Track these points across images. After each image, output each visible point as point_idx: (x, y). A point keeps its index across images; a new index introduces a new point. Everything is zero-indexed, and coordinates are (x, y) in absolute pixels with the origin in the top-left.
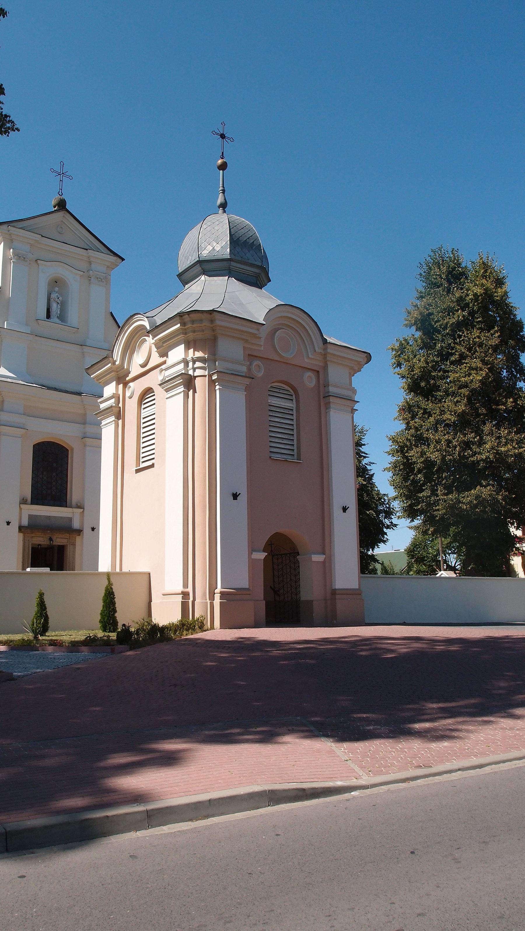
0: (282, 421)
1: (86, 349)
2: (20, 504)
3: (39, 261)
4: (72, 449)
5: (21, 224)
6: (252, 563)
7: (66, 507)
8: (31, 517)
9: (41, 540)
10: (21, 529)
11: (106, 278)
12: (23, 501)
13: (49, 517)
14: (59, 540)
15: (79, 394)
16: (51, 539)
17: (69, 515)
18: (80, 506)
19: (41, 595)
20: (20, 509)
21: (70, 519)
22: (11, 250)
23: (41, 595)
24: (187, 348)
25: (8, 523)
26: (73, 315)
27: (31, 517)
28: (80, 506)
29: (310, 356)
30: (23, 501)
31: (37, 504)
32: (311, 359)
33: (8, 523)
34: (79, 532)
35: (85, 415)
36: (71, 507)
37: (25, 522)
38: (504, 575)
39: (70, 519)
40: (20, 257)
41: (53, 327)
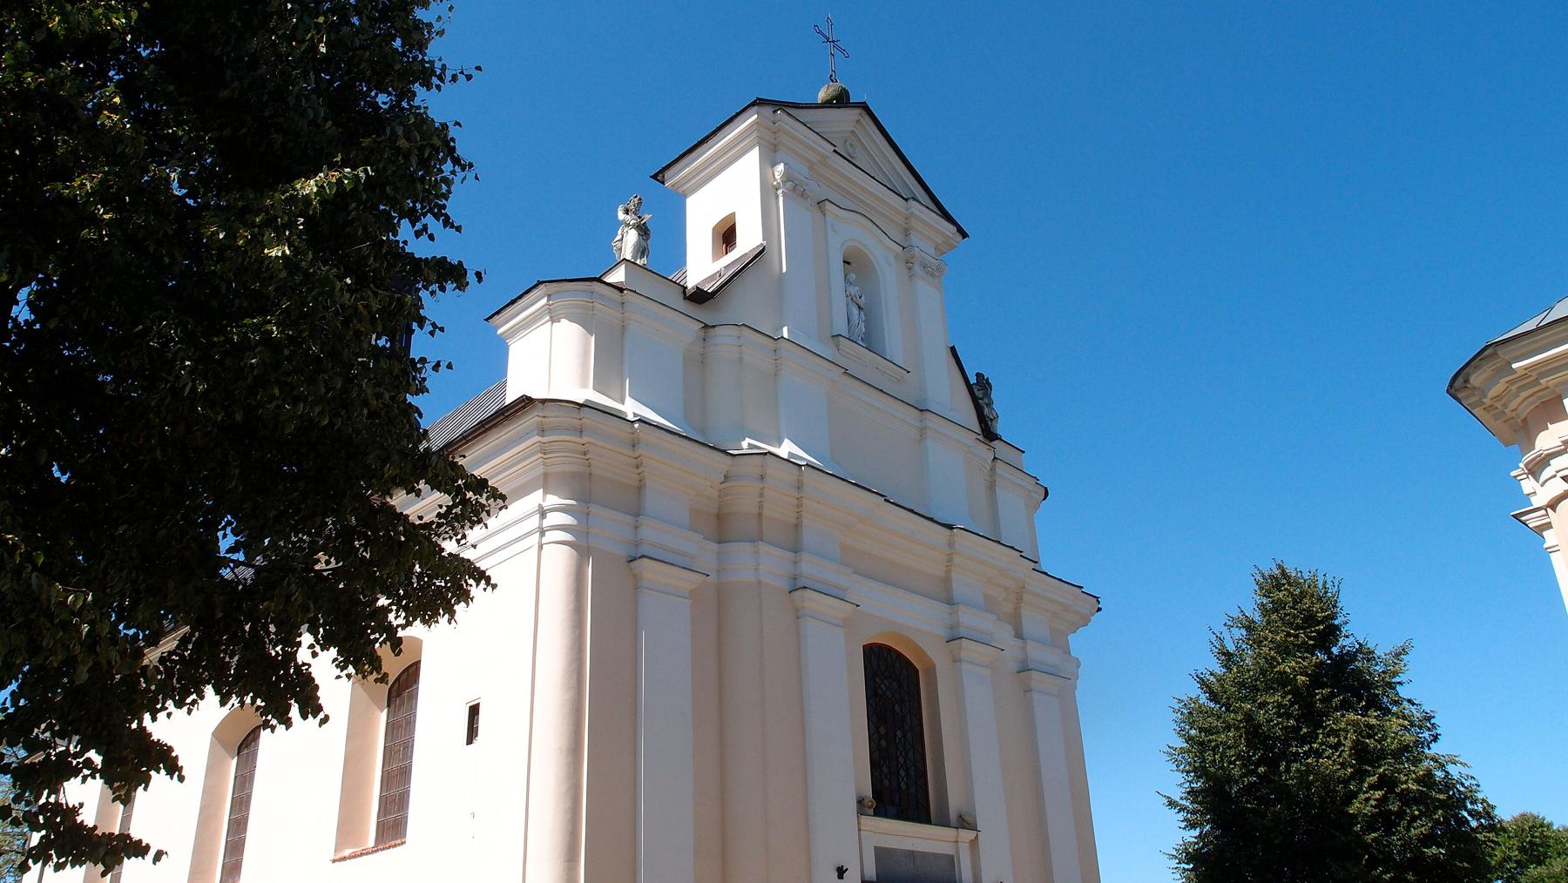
1: (932, 422)
3: (828, 206)
4: (931, 669)
5: (791, 111)
7: (928, 821)
8: (881, 853)
11: (939, 269)
13: (912, 854)
15: (950, 527)
17: (944, 848)
18: (965, 822)
21: (951, 860)
22: (781, 167)
24: (545, 493)
27: (881, 853)
28: (965, 822)
31: (886, 815)
36: (944, 822)
38: (920, 821)
40: (796, 188)
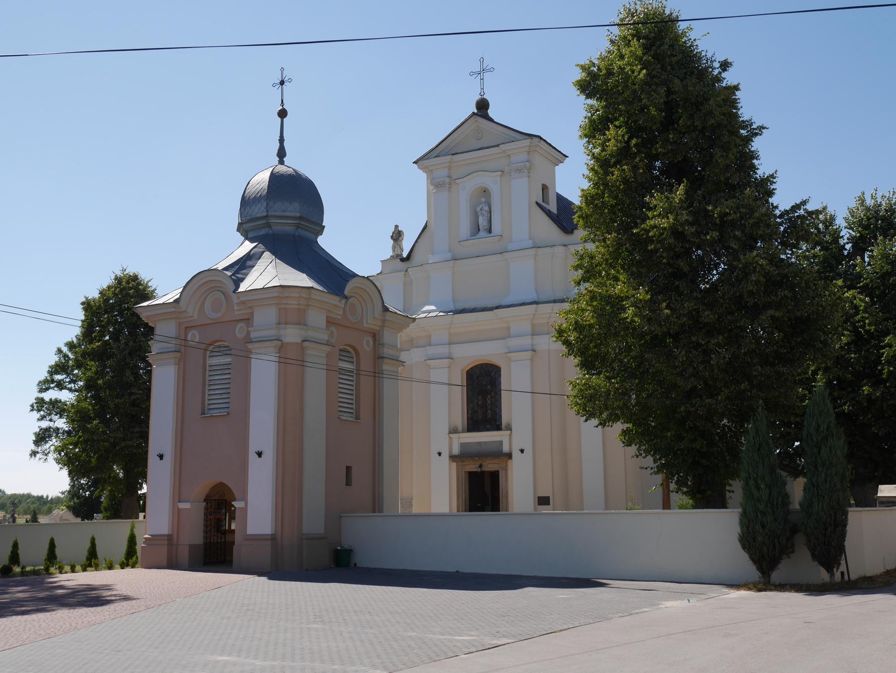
0: (222, 377)
2: (450, 433)
6: (244, 498)
8: (463, 445)
9: (473, 467)
10: (453, 458)
12: (453, 431)
14: (490, 466)
16: (481, 466)
19: (15, 546)
20: (451, 438)
23: (15, 546)
25: (440, 454)
26: (496, 227)
27: (463, 445)
28: (509, 428)
29: (369, 321)
30: (453, 431)
32: (370, 323)
33: (440, 454)
34: (509, 456)
35: (509, 328)
37: (456, 451)
39: (501, 443)
41: (483, 242)
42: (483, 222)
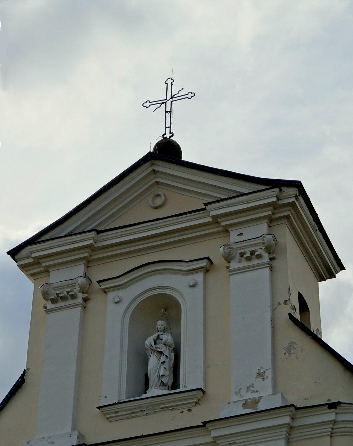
42: (156, 366)
